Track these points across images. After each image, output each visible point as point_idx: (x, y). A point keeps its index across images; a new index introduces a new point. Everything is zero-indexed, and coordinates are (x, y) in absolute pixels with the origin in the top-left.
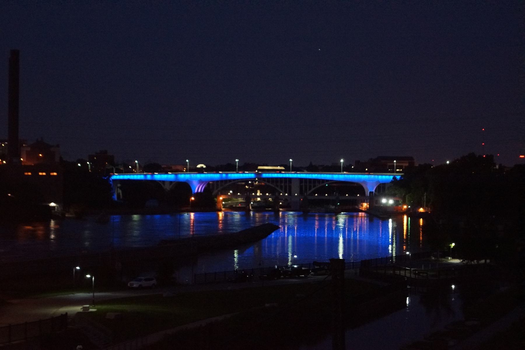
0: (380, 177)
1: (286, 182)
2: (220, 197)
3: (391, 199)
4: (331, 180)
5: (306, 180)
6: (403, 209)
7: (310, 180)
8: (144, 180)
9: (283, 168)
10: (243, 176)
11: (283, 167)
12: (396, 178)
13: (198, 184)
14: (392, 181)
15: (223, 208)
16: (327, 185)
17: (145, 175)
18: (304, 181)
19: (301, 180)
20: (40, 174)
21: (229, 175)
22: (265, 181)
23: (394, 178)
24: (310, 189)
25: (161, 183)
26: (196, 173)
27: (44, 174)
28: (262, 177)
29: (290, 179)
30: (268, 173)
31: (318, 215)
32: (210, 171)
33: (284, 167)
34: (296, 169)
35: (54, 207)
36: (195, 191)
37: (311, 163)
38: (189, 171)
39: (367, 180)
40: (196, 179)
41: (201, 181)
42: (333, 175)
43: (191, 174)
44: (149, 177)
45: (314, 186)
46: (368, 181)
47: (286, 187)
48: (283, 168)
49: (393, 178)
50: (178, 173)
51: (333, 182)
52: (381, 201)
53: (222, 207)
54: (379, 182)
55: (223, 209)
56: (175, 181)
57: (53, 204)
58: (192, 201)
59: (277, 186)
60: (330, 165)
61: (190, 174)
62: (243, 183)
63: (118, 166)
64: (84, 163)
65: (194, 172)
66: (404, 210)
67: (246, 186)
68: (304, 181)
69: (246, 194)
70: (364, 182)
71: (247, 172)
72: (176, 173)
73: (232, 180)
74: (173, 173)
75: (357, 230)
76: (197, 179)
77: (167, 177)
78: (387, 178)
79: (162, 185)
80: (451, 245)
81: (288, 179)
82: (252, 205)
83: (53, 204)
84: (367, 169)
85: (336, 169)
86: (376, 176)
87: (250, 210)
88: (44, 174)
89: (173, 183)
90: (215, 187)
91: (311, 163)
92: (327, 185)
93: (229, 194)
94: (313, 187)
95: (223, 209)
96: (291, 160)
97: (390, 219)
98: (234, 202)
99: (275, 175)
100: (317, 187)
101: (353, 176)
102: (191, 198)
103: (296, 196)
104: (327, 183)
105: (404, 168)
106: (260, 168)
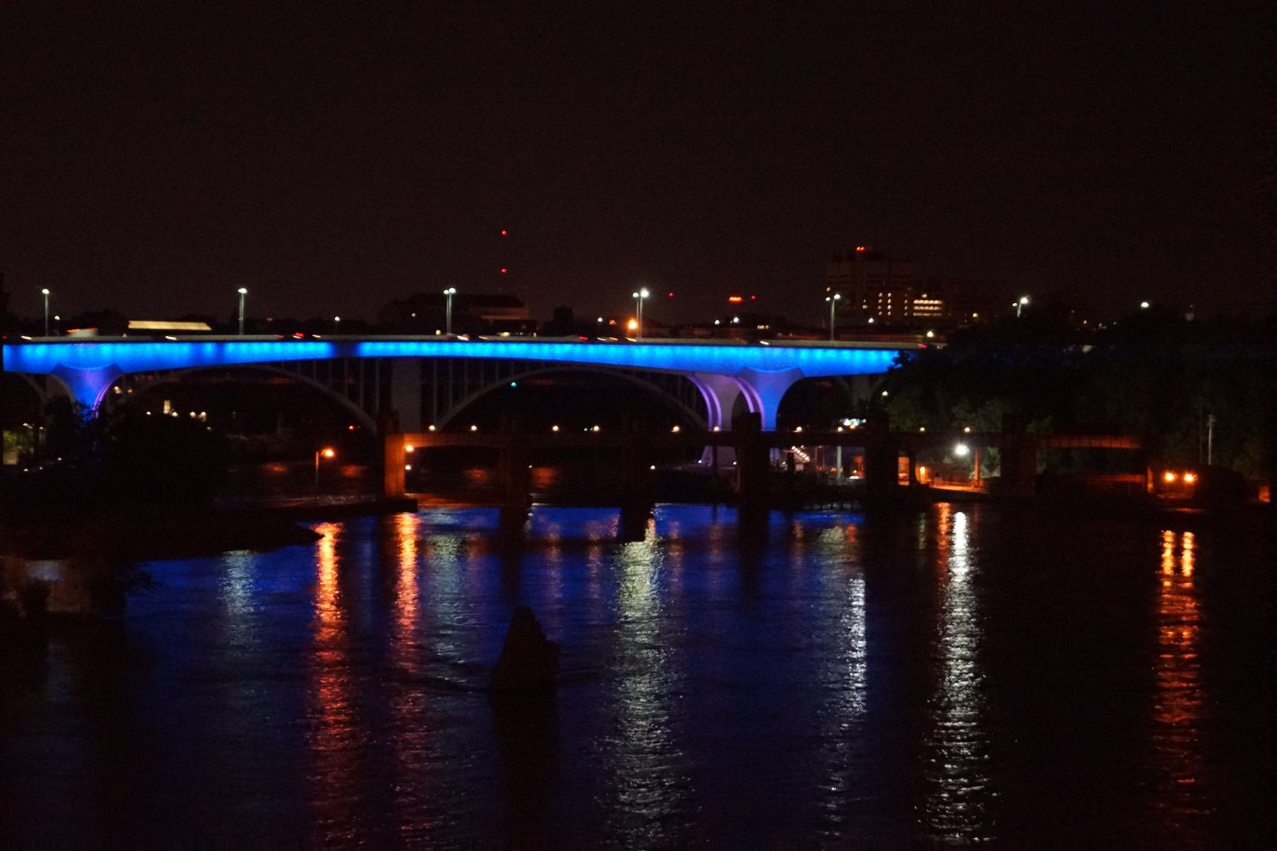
0: (804, 354)
2: (1164, 476)
3: (1170, 472)
14: (891, 368)
17: (220, 353)
21: (230, 348)
25: (31, 382)
26: (275, 337)
28: (359, 355)
33: (209, 324)
34: (256, 328)
39: (756, 367)
40: (97, 362)
42: (653, 347)
46: (760, 371)
52: (331, 449)
75: (417, 749)
77: (47, 357)
79: (37, 387)
81: (314, 363)
86: (791, 352)
92: (513, 384)
96: (46, 291)
106: (134, 325)
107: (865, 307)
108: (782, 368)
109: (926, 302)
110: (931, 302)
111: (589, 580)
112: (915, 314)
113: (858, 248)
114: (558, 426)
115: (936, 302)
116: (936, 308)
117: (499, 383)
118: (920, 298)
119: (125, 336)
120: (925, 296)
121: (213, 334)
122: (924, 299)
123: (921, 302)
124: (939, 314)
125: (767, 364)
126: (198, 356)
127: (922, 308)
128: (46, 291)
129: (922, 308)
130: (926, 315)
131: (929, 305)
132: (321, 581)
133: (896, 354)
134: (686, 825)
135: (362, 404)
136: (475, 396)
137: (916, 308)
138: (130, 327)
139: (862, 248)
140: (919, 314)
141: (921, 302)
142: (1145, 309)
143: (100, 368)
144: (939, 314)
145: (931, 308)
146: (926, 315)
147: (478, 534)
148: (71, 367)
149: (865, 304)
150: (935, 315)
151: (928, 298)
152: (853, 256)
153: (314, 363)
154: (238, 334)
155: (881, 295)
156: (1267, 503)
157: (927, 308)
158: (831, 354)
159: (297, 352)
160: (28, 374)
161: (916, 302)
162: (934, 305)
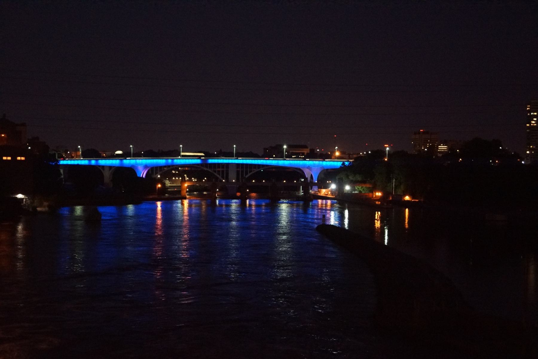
5: (242, 165)
7: (247, 165)
9: (203, 154)
16: (262, 170)
17: (90, 160)
19: (238, 165)
20: (5, 158)
21: (175, 161)
24: (247, 174)
25: (100, 168)
27: (9, 158)
31: (319, 206)
32: (312, 158)
35: (22, 199)
37: (221, 150)
38: (133, 157)
40: (141, 164)
41: (146, 167)
44: (93, 162)
45: (250, 172)
47: (223, 171)
48: (203, 154)
49: (342, 164)
50: (98, 159)
54: (324, 168)
55: (188, 196)
56: (119, 166)
57: (20, 196)
58: (159, 188)
59: (215, 172)
60: (241, 152)
61: (135, 159)
63: (337, 151)
65: (155, 157)
67: (173, 171)
70: (137, 164)
71: (308, 160)
74: (310, 159)
76: (143, 165)
81: (240, 165)
83: (20, 196)
85: (229, 155)
86: (321, 162)
87: (216, 198)
88: (9, 158)
89: (113, 169)
90: (154, 172)
91: (221, 150)
92: (262, 170)
93: (204, 180)
94: (249, 173)
95: (188, 196)
96: (181, 146)
97: (237, 196)
100: (253, 172)
101: (157, 160)
102: (158, 185)
105: (305, 154)
107: (423, 148)
109: (442, 147)
110: (444, 147)
112: (439, 150)
113: (421, 130)
115: (446, 147)
116: (446, 148)
117: (258, 170)
118: (440, 145)
119: (179, 157)
120: (442, 145)
122: (442, 146)
123: (441, 147)
124: (447, 150)
125: (314, 165)
126: (167, 163)
127: (441, 148)
128: (181, 146)
129: (441, 148)
130: (443, 150)
131: (443, 148)
132: (279, 223)
133: (342, 163)
134: (333, 298)
135: (221, 175)
136: (251, 173)
137: (439, 148)
139: (422, 130)
140: (440, 150)
141: (441, 147)
142: (30, 149)
143: (143, 166)
144: (447, 150)
145: (444, 148)
146: (443, 150)
148: (137, 166)
149: (423, 147)
150: (445, 150)
151: (443, 146)
152: (419, 133)
153: (240, 165)
155: (428, 144)
156: (408, 209)
157: (443, 148)
161: (439, 146)
162: (445, 148)
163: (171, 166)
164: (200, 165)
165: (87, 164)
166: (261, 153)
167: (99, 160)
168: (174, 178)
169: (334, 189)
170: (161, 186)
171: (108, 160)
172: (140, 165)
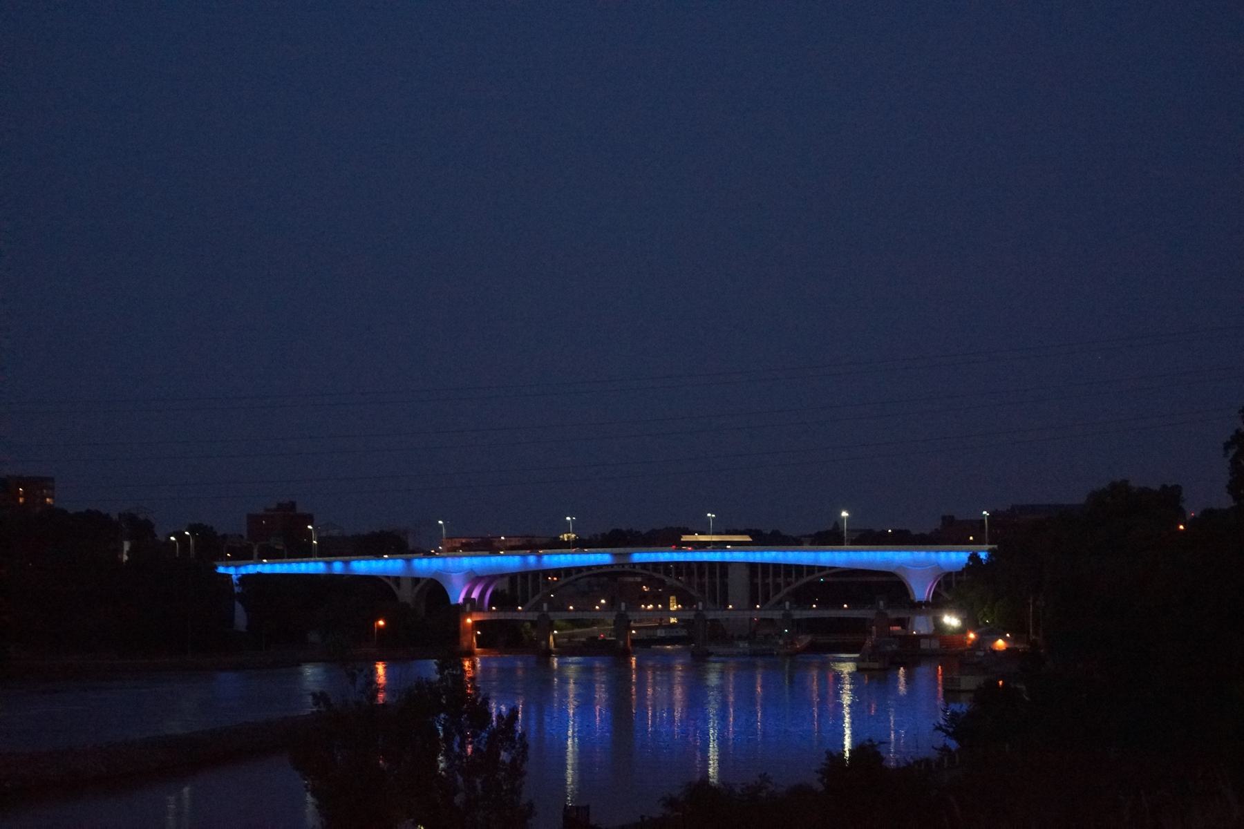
0: (943, 555)
1: (701, 575)
3: (956, 617)
4: (831, 568)
6: (969, 642)
8: (326, 574)
10: (754, 559)
11: (747, 536)
12: (978, 557)
13: (464, 585)
14: (967, 564)
15: (478, 648)
17: (329, 563)
18: (760, 570)
19: (752, 566)
21: (546, 558)
22: (660, 573)
23: (974, 557)
29: (724, 565)
30: (648, 552)
33: (751, 537)
36: (458, 601)
41: (475, 578)
43: (551, 554)
44: (338, 567)
46: (910, 567)
48: (747, 538)
49: (970, 558)
51: (834, 571)
53: (475, 646)
54: (475, 573)
58: (379, 627)
62: (639, 579)
64: (179, 535)
66: (971, 645)
68: (760, 570)
69: (695, 606)
70: (445, 573)
72: (347, 558)
73: (584, 570)
74: (507, 552)
76: (460, 572)
78: (956, 558)
80: (501, 758)
81: (782, 567)
82: (555, 636)
84: (971, 538)
85: (831, 537)
86: (933, 555)
89: (421, 584)
96: (845, 514)
98: (606, 627)
99: (716, 556)
103: (385, 620)
104: (822, 574)
108: (934, 564)
111: (632, 695)
114: (605, 600)
121: (753, 545)
128: (440, 522)
138: (682, 540)
143: (462, 573)
147: (576, 666)
148: (445, 573)
153: (782, 567)
154: (843, 545)
158: (569, 557)
159: (560, 563)
160: (388, 577)
163: (574, 572)
164: (651, 566)
165: (324, 573)
166: (724, 532)
167: (354, 560)
168: (643, 606)
169: (953, 627)
170: (976, 637)
171: (511, 557)
172: (456, 573)
